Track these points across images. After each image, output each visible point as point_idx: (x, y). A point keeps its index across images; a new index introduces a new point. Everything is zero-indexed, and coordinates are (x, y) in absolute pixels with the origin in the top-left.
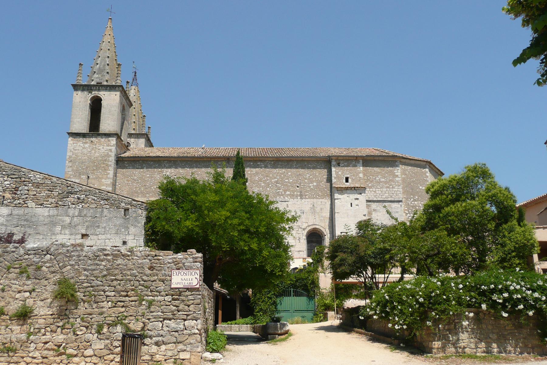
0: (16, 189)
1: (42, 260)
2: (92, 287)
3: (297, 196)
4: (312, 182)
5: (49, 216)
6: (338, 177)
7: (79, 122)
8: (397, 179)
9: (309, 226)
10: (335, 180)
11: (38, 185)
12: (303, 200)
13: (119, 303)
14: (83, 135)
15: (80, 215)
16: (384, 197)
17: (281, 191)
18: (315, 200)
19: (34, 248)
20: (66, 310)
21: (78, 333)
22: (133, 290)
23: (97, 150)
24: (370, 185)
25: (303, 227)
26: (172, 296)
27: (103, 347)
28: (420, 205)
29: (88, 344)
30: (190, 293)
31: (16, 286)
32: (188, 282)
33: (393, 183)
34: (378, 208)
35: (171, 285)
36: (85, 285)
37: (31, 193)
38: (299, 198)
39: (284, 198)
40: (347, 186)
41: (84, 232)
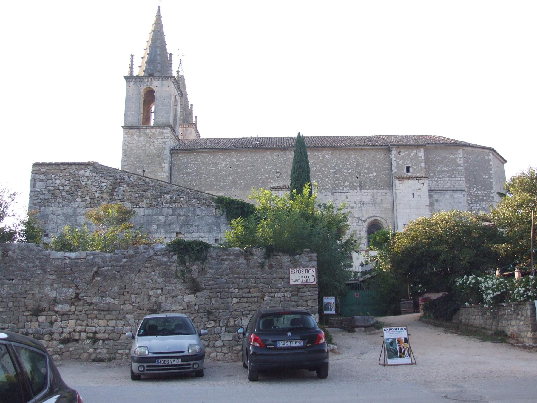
0: (113, 190)
1: (171, 260)
2: (217, 284)
3: (357, 187)
4: (372, 173)
5: (145, 215)
6: (398, 167)
7: (132, 114)
8: (460, 168)
9: (369, 218)
10: (396, 170)
11: (133, 186)
12: (363, 191)
13: (242, 299)
14: (138, 128)
15: (173, 214)
16: (447, 186)
17: (340, 181)
18: (375, 191)
19: (162, 249)
20: (195, 305)
21: (208, 326)
22: (254, 287)
23: (151, 144)
24: (431, 174)
25: (363, 219)
26: (291, 291)
27: (231, 339)
28: (484, 195)
29: (218, 336)
30: (307, 290)
31: (148, 284)
32: (306, 279)
33: (455, 172)
34: (440, 198)
35: (289, 282)
36: (211, 282)
37: (127, 194)
38: (358, 188)
39: (343, 189)
40: (408, 176)
41: (178, 230)
